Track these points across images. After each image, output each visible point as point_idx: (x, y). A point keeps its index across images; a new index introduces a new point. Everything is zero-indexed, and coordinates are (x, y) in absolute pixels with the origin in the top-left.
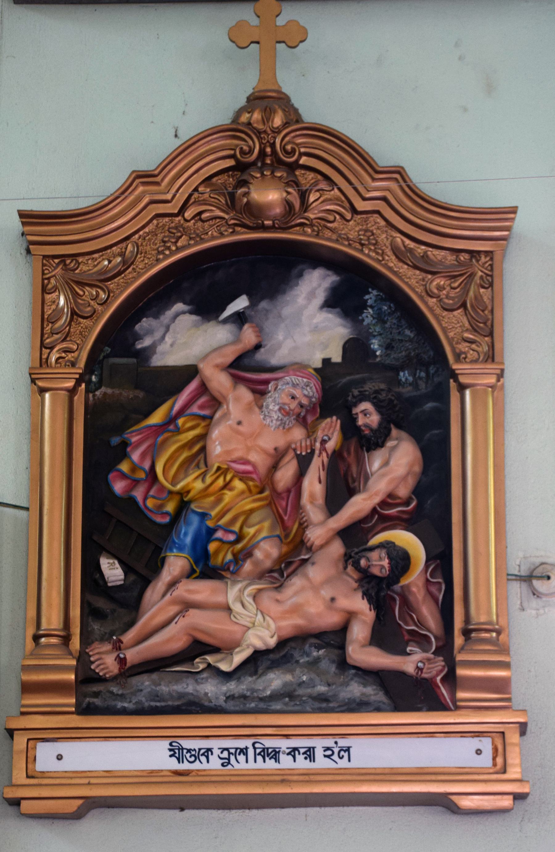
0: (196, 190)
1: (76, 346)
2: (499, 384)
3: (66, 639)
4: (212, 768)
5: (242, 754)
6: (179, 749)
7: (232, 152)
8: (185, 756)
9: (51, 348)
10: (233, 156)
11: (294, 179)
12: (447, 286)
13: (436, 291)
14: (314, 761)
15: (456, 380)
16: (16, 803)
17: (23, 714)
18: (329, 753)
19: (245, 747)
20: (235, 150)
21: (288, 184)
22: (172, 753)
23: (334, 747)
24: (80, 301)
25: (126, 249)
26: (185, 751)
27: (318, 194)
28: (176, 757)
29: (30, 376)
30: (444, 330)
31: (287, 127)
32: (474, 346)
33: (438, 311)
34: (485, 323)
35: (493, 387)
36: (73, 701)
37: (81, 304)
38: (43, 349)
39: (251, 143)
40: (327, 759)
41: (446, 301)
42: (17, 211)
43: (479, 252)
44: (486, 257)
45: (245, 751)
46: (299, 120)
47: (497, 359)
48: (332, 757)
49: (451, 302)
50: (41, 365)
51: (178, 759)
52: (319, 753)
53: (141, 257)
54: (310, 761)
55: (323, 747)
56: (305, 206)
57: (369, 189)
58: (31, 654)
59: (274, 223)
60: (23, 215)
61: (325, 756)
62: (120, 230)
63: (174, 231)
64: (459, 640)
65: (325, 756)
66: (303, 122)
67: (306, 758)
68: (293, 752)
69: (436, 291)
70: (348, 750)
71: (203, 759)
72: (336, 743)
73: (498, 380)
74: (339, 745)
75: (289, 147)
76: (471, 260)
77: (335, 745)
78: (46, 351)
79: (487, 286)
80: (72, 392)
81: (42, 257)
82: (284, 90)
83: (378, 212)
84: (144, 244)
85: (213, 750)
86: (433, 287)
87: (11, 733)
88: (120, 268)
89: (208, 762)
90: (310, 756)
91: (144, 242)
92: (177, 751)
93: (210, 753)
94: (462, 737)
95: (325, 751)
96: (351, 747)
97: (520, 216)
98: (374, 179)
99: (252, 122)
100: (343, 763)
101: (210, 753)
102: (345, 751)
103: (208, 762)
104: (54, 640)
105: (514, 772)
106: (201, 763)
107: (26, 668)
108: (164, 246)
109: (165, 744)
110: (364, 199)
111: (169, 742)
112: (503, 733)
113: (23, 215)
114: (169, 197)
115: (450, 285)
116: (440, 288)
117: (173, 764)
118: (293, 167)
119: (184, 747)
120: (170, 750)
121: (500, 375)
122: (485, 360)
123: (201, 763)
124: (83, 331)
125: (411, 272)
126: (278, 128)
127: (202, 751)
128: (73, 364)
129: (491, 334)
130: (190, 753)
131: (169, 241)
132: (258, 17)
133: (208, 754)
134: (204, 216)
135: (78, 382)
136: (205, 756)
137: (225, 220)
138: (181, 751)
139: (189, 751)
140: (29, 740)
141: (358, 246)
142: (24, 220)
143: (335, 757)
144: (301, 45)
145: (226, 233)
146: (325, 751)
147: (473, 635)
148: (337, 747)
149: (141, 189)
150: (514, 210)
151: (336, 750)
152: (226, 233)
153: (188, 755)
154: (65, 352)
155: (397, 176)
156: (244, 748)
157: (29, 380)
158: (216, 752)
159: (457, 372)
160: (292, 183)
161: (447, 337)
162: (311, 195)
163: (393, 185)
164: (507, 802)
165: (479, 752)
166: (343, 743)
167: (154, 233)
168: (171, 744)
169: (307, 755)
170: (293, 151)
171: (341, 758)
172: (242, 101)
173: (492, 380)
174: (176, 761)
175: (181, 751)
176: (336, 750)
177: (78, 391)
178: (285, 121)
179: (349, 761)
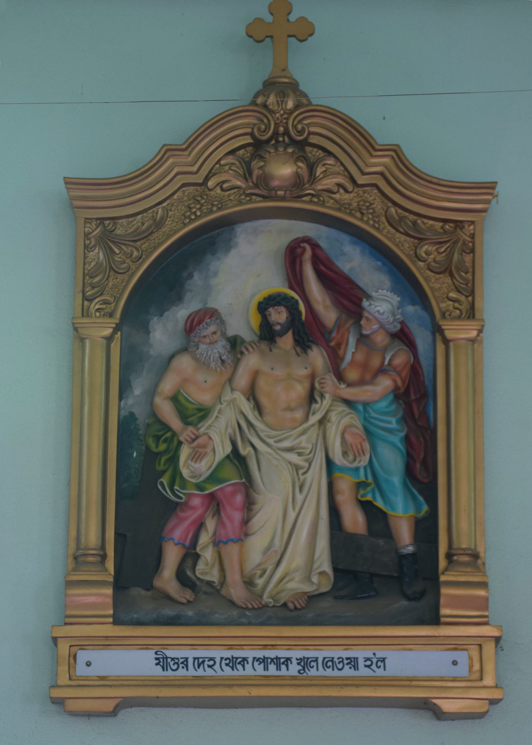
0: (218, 162)
1: (113, 298)
2: (479, 338)
3: (104, 557)
4: (247, 674)
5: (272, 663)
6: (163, 658)
7: (249, 130)
8: (169, 663)
11: (302, 154)
12: (434, 251)
13: (424, 255)
14: (358, 670)
16: (59, 702)
17: (66, 624)
18: (368, 663)
19: (275, 657)
20: (253, 129)
21: (297, 160)
22: (157, 661)
23: (372, 658)
24: (116, 259)
25: (157, 213)
26: (169, 660)
28: (161, 665)
29: (73, 326)
30: (432, 289)
31: (299, 109)
32: (456, 305)
34: (466, 285)
35: (473, 341)
36: (111, 612)
37: (118, 261)
38: (85, 300)
39: (265, 120)
40: (367, 669)
42: (63, 178)
43: (461, 222)
45: (275, 660)
46: (310, 104)
47: (477, 316)
48: (372, 667)
50: (83, 316)
52: (361, 663)
53: (170, 221)
54: (355, 670)
55: (364, 658)
56: (313, 178)
57: (368, 165)
58: (74, 570)
59: (285, 194)
60: (69, 182)
61: (366, 666)
62: (209, 159)
63: (199, 199)
64: (442, 563)
65: (366, 666)
67: (350, 668)
69: (424, 255)
70: (383, 660)
71: (239, 667)
72: (374, 654)
73: (478, 335)
74: (377, 656)
75: (300, 127)
76: (455, 228)
77: (373, 656)
78: (86, 303)
79: (468, 251)
80: (109, 339)
81: (84, 219)
82: (295, 77)
83: (375, 186)
84: (173, 209)
85: (292, 659)
86: (422, 253)
87: (55, 640)
88: (152, 229)
89: (244, 670)
90: (354, 667)
91: (173, 207)
92: (161, 660)
93: (289, 662)
94: (405, 650)
95: (365, 661)
96: (386, 658)
97: (497, 189)
98: (372, 156)
99: (268, 103)
100: (380, 672)
101: (246, 662)
102: (314, 661)
103: (244, 670)
104: (91, 559)
105: (489, 680)
106: (238, 670)
107: (70, 584)
108: (190, 211)
109: (150, 655)
110: (363, 173)
111: (154, 651)
112: (480, 645)
115: (437, 250)
116: (428, 253)
117: (158, 671)
118: (305, 143)
119: (168, 656)
120: (156, 659)
121: (480, 331)
122: (468, 316)
123: (238, 670)
124: (119, 285)
125: (403, 238)
126: (289, 110)
127: (239, 660)
129: (472, 293)
130: (174, 661)
131: (194, 207)
132: (272, 14)
133: (287, 663)
134: (225, 186)
135: (117, 329)
136: (241, 665)
137: (243, 190)
138: (165, 660)
139: (173, 659)
140: (71, 646)
141: (358, 215)
142: (68, 186)
143: (374, 667)
144: (310, 38)
146: (365, 661)
147: (455, 558)
148: (375, 657)
149: (171, 161)
151: (375, 661)
152: (244, 201)
153: (172, 663)
154: (105, 303)
156: (274, 658)
157: (72, 328)
158: (295, 662)
159: (444, 327)
160: (302, 158)
161: (434, 296)
162: (318, 169)
165: (455, 663)
166: (380, 654)
167: (180, 200)
168: (156, 653)
169: (184, 664)
170: (303, 130)
171: (379, 667)
172: (260, 86)
173: (474, 334)
174: (161, 669)
175: (165, 660)
176: (375, 661)
177: (114, 338)
178: (296, 104)
179: (385, 669)
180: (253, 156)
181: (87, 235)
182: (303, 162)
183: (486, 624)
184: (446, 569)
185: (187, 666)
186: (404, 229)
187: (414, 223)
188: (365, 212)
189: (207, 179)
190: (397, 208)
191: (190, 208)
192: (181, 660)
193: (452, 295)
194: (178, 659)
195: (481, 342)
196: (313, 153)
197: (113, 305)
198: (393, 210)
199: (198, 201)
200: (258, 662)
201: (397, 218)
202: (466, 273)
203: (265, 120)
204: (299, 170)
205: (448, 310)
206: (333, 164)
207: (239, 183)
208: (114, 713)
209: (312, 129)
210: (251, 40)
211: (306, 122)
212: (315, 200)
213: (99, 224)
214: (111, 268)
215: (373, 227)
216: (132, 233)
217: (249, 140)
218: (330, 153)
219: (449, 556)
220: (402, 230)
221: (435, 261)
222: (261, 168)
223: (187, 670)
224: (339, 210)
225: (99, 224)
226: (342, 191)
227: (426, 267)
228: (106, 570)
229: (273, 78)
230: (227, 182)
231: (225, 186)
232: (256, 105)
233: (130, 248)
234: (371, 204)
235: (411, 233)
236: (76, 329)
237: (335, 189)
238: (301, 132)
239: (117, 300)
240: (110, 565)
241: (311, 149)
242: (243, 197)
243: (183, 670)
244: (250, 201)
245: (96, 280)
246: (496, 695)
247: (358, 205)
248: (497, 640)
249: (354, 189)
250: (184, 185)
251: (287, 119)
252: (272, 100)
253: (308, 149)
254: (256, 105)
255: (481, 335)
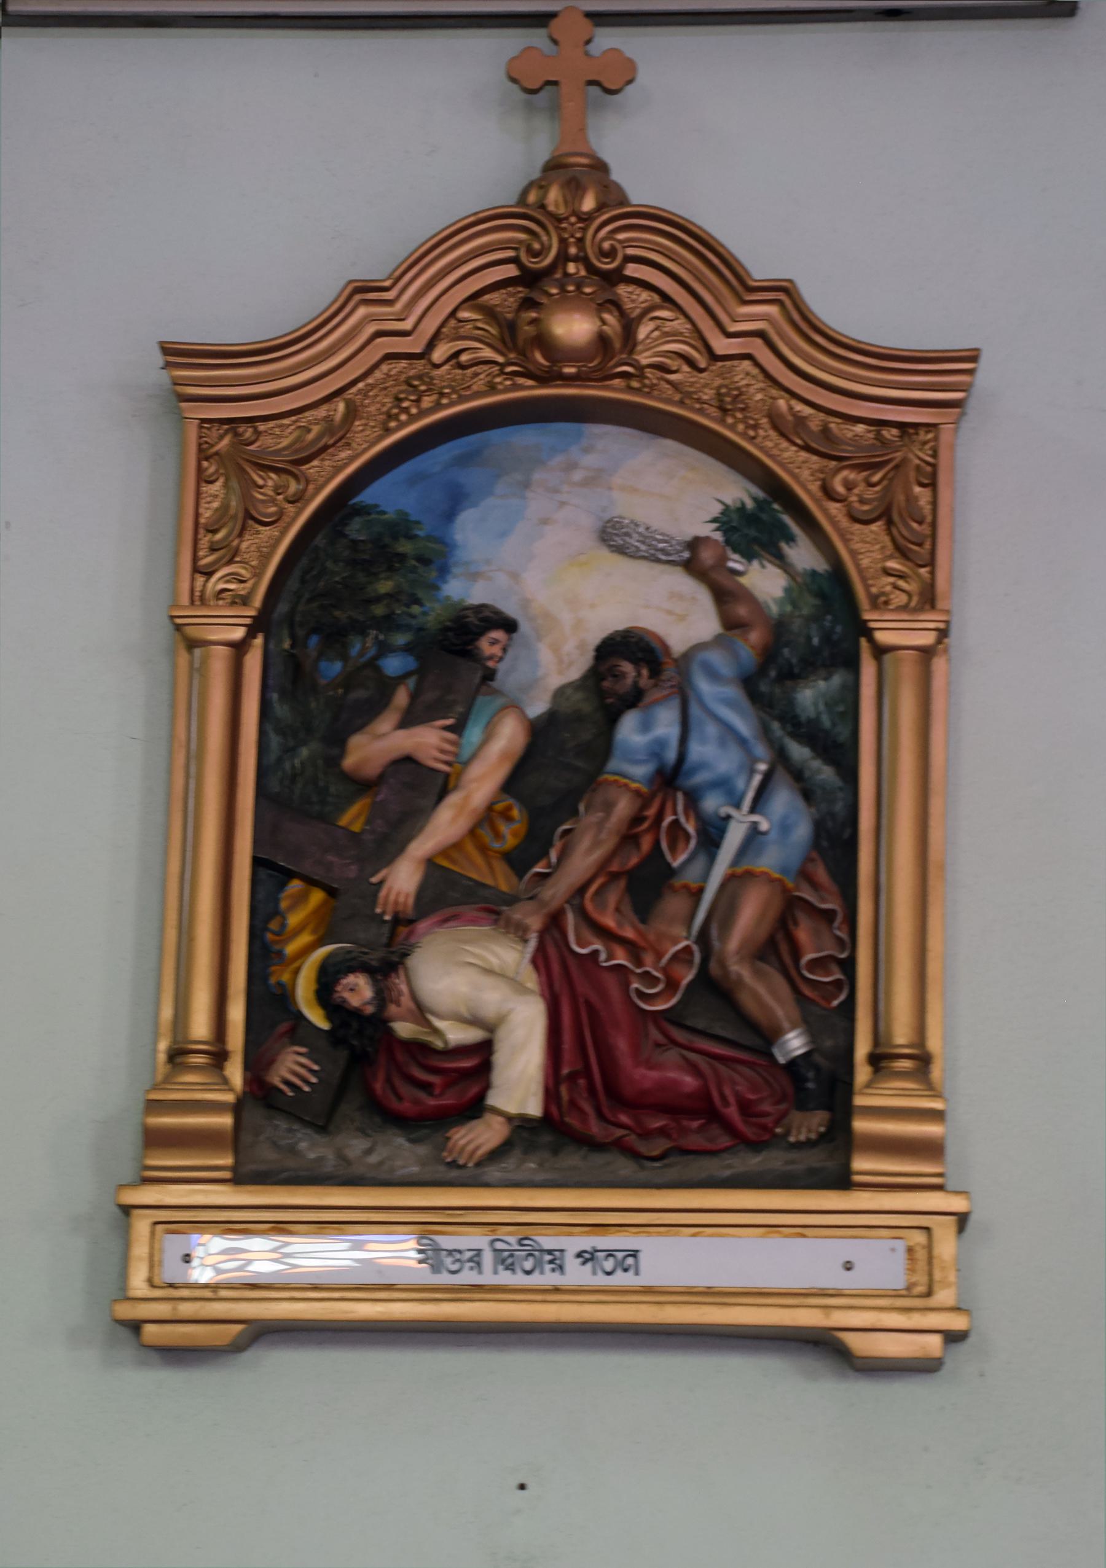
0: (453, 314)
3: (219, 1057)
7: (510, 254)
9: (209, 574)
10: (515, 260)
15: (871, 640)
16: (135, 1326)
21: (601, 307)
27: (651, 325)
33: (845, 522)
35: (926, 653)
39: (545, 238)
41: (857, 505)
44: (927, 432)
46: (624, 201)
47: (940, 604)
49: (866, 508)
50: (192, 602)
51: (432, 1266)
58: (167, 1079)
60: (168, 350)
63: (416, 383)
64: (862, 1073)
66: (630, 205)
68: (587, 1257)
69: (840, 489)
70: (634, 1254)
73: (939, 641)
75: (606, 245)
78: (200, 580)
80: (239, 648)
87: (127, 1210)
105: (944, 1296)
107: (153, 1106)
108: (399, 407)
113: (168, 350)
114: (407, 325)
116: (849, 486)
118: (615, 278)
121: (943, 633)
128: (245, 601)
129: (931, 563)
131: (406, 399)
134: (464, 358)
135: (252, 631)
139: (450, 1252)
145: (500, 387)
150: (973, 356)
155: (782, 296)
157: (170, 628)
159: (873, 625)
163: (773, 310)
164: (934, 1343)
173: (927, 639)
179: (637, 1273)
180: (529, 303)
181: (204, 453)
182: (610, 312)
183: (939, 1188)
184: (869, 1085)
185: (479, 1264)
186: (802, 439)
187: (825, 431)
188: (729, 407)
189: (431, 345)
190: (793, 402)
191: (399, 400)
192: (469, 1254)
193: (892, 564)
194: (460, 1252)
195: (946, 651)
196: (633, 298)
197: (249, 585)
198: (782, 403)
199: (415, 387)
200: (580, 1260)
201: (790, 418)
202: (920, 523)
203: (545, 238)
204: (605, 328)
205: (883, 594)
206: (671, 318)
207: (487, 353)
208: (238, 1347)
209: (630, 251)
210: (515, 87)
211: (621, 236)
212: (635, 384)
213: (227, 432)
214: (248, 516)
215: (743, 435)
216: (284, 449)
217: (511, 271)
218: (666, 298)
219: (876, 1060)
220: (799, 442)
221: (862, 501)
222: (534, 321)
223: (637, 1273)
224: (681, 403)
225: (227, 432)
226: (686, 368)
227: (844, 511)
228: (225, 1081)
229: (561, 156)
230: (467, 352)
231: (464, 358)
232: (527, 206)
233: (284, 477)
234: (741, 394)
235: (814, 445)
236: (178, 628)
237: (673, 364)
238: (611, 254)
239: (258, 574)
240: (235, 1073)
241: (630, 288)
242: (498, 380)
243: (471, 1272)
244: (516, 387)
245: (219, 536)
246: (958, 1323)
247: (719, 394)
248: (962, 1220)
249: (709, 365)
250: (389, 357)
251: (584, 230)
252: (554, 195)
253: (623, 290)
254: (527, 206)
255: (946, 640)
